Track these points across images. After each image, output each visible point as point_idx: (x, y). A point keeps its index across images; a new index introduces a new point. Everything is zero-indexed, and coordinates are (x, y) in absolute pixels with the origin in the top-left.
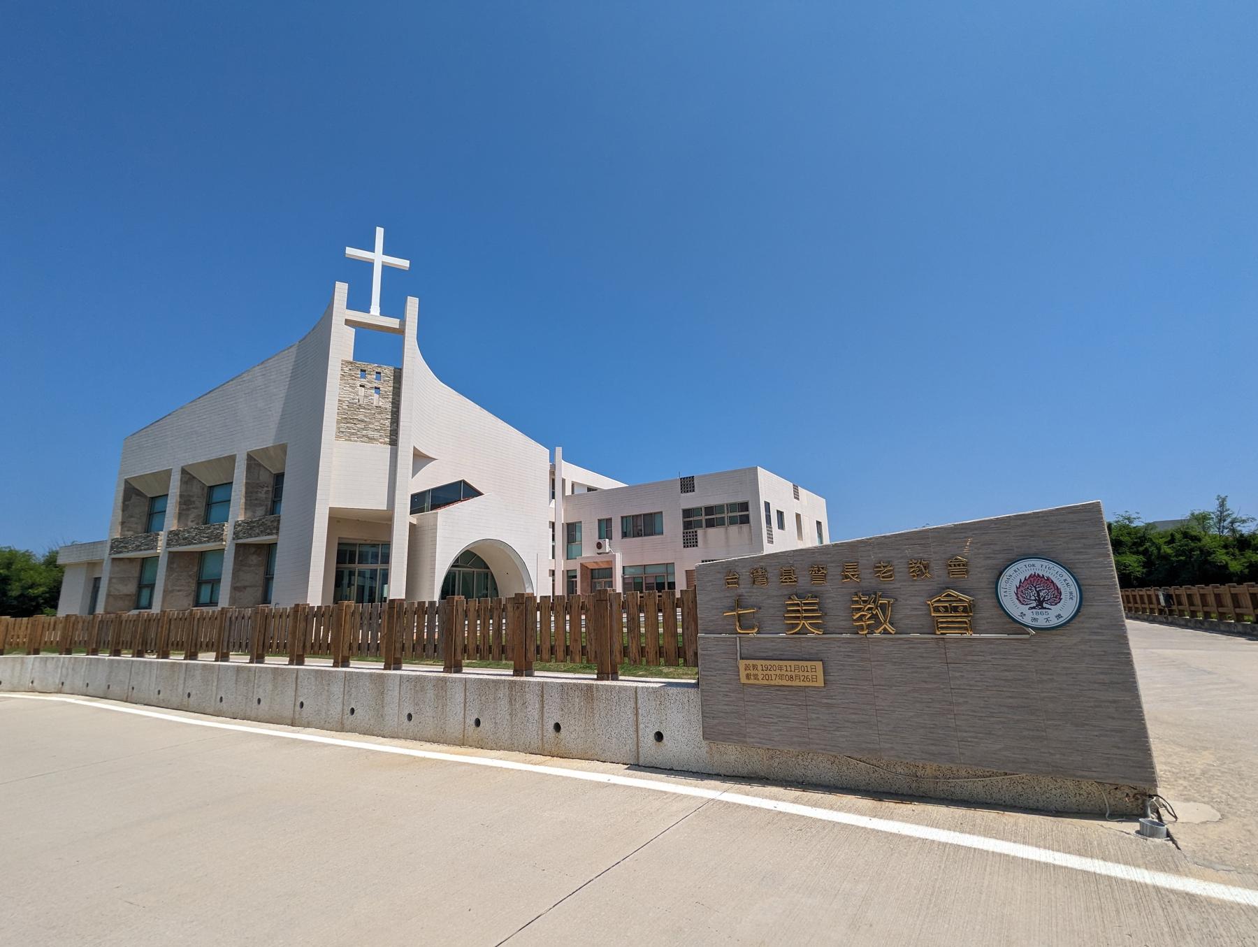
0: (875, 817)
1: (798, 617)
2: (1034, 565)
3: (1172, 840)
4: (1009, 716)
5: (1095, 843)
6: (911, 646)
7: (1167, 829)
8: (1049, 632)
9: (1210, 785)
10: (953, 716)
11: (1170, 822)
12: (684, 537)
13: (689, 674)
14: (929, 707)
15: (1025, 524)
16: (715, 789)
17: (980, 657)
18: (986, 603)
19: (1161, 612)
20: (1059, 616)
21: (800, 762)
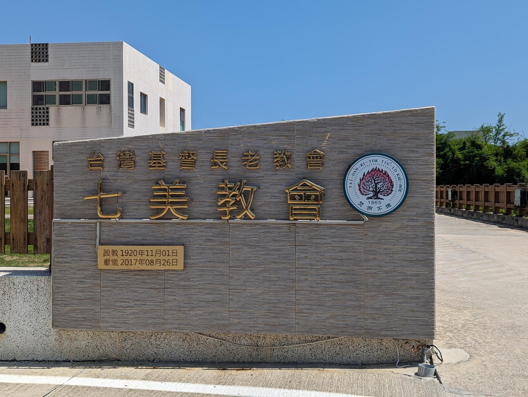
0: (219, 384)
1: (164, 203)
2: (376, 161)
3: (438, 378)
4: (339, 290)
5: (387, 385)
6: (267, 230)
7: (436, 370)
8: (385, 219)
9: (466, 335)
10: (294, 292)
11: (438, 365)
12: (33, 113)
13: (36, 262)
14: (275, 285)
15: (375, 123)
16: (63, 375)
17: (322, 240)
18: (334, 192)
19: (447, 205)
20: (388, 205)
21: (153, 342)
